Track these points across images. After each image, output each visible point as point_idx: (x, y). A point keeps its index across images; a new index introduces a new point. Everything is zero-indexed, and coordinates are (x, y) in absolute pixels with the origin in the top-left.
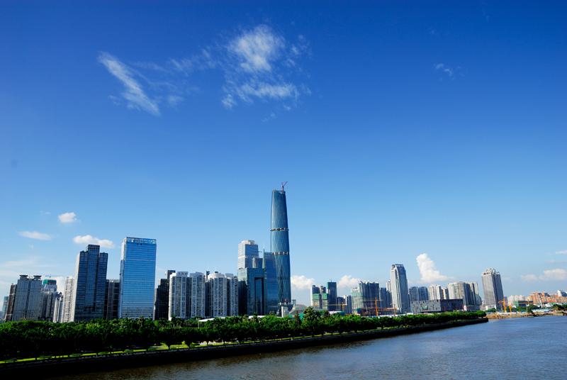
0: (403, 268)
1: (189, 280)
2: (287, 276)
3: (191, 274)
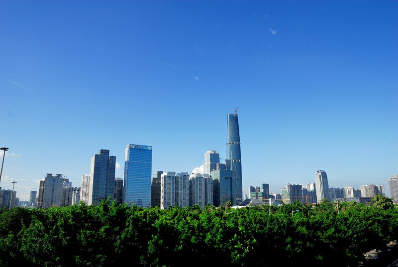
0: (325, 173)
1: (176, 178)
2: (240, 178)
3: (178, 174)
